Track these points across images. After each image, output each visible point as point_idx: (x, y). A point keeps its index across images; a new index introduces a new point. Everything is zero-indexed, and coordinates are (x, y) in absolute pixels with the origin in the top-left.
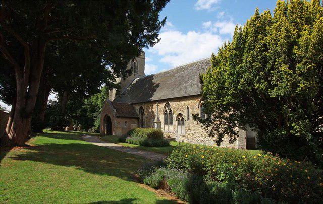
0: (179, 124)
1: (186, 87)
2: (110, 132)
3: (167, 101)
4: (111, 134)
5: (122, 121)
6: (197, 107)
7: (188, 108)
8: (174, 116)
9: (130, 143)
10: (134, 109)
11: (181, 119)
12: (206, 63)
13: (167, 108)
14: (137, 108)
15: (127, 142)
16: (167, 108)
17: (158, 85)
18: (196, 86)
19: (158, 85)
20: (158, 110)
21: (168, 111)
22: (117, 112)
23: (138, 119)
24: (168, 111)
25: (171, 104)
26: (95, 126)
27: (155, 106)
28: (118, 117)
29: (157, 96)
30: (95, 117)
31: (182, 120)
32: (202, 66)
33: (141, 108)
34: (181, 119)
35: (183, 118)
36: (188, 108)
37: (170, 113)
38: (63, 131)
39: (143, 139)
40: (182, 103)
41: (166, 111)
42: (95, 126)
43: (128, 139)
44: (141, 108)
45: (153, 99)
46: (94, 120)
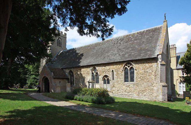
0: (105, 83)
1: (108, 56)
2: (47, 89)
3: (94, 66)
4: (49, 91)
5: (57, 81)
6: (121, 70)
7: (113, 71)
8: (101, 78)
9: (80, 100)
10: (65, 72)
11: (106, 79)
12: (120, 39)
13: (93, 72)
14: (67, 71)
15: (76, 100)
16: (93, 72)
17: (82, 55)
18: (118, 55)
19: (82, 55)
20: (87, 74)
21: (95, 74)
22: (54, 74)
23: (68, 79)
24: (95, 74)
25: (97, 68)
26: (27, 84)
27: (83, 70)
28: (54, 78)
29: (83, 62)
30: (27, 78)
31: (107, 80)
32: (118, 41)
33: (71, 72)
34: (106, 79)
35: (108, 79)
36: (113, 71)
37: (96, 75)
38: (56, 57)
39: (95, 98)
40: (108, 67)
41: (93, 73)
42: (27, 84)
43: (76, 97)
44: (71, 72)
45: (81, 64)
46: (26, 80)
